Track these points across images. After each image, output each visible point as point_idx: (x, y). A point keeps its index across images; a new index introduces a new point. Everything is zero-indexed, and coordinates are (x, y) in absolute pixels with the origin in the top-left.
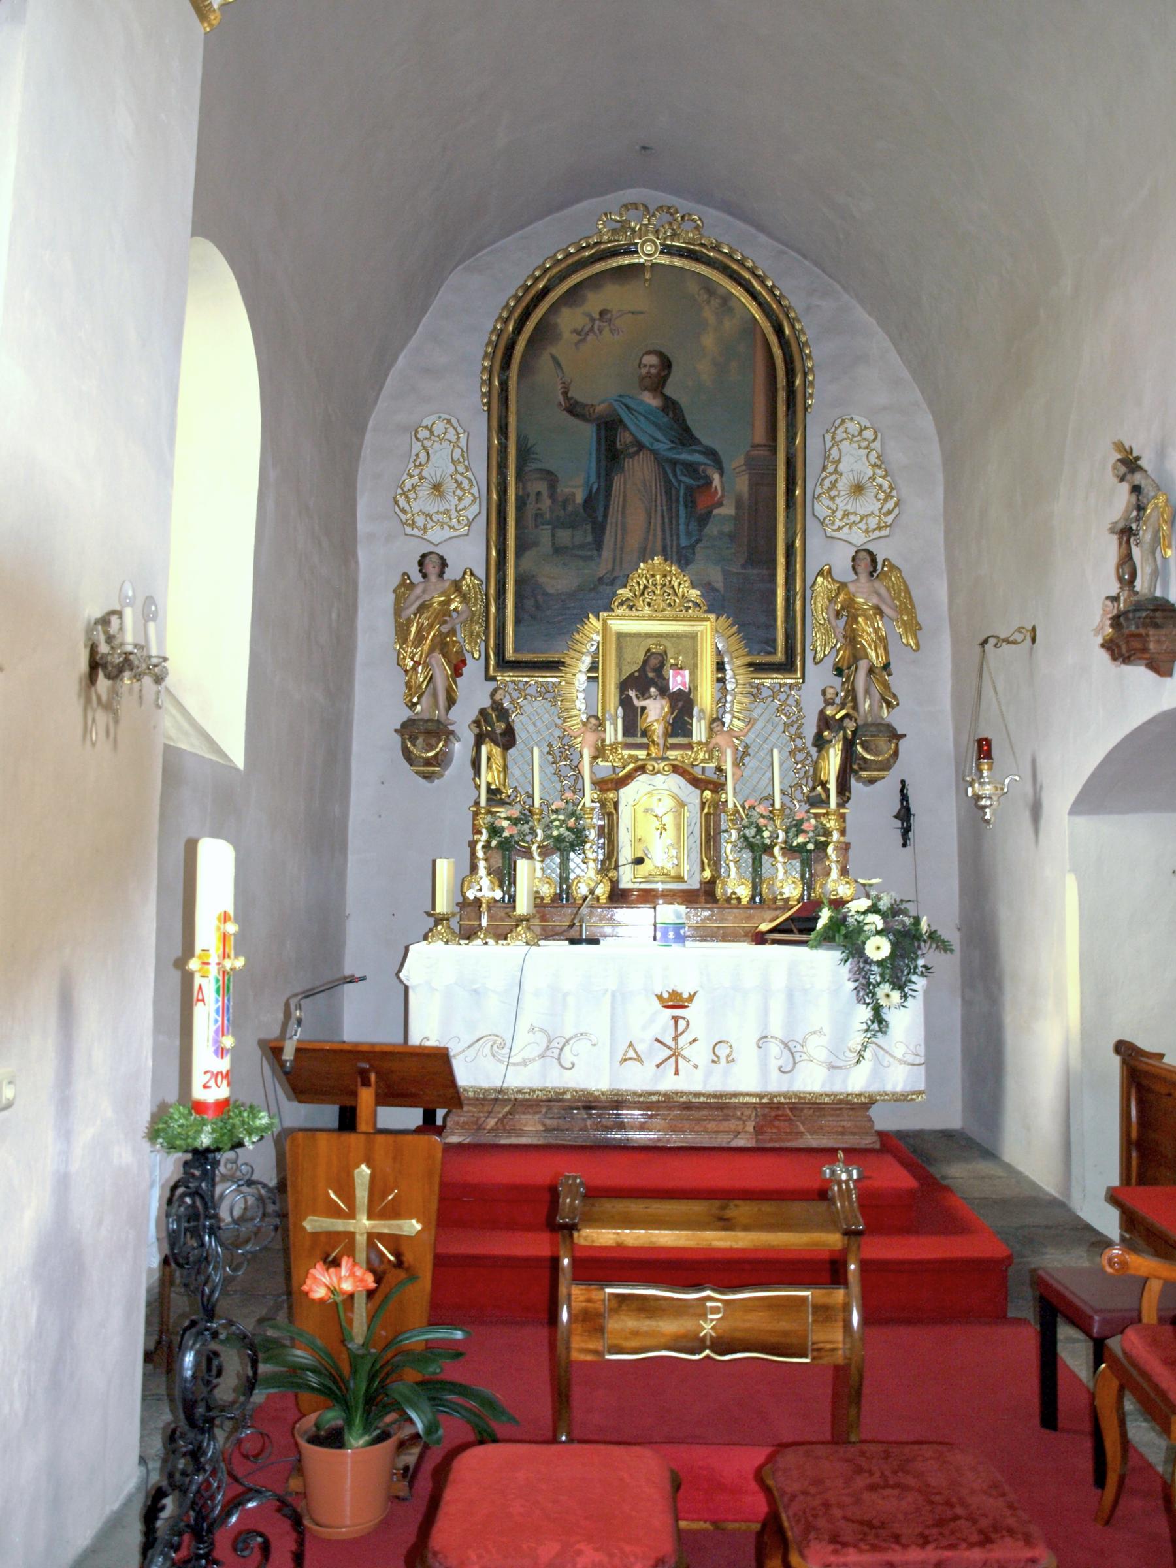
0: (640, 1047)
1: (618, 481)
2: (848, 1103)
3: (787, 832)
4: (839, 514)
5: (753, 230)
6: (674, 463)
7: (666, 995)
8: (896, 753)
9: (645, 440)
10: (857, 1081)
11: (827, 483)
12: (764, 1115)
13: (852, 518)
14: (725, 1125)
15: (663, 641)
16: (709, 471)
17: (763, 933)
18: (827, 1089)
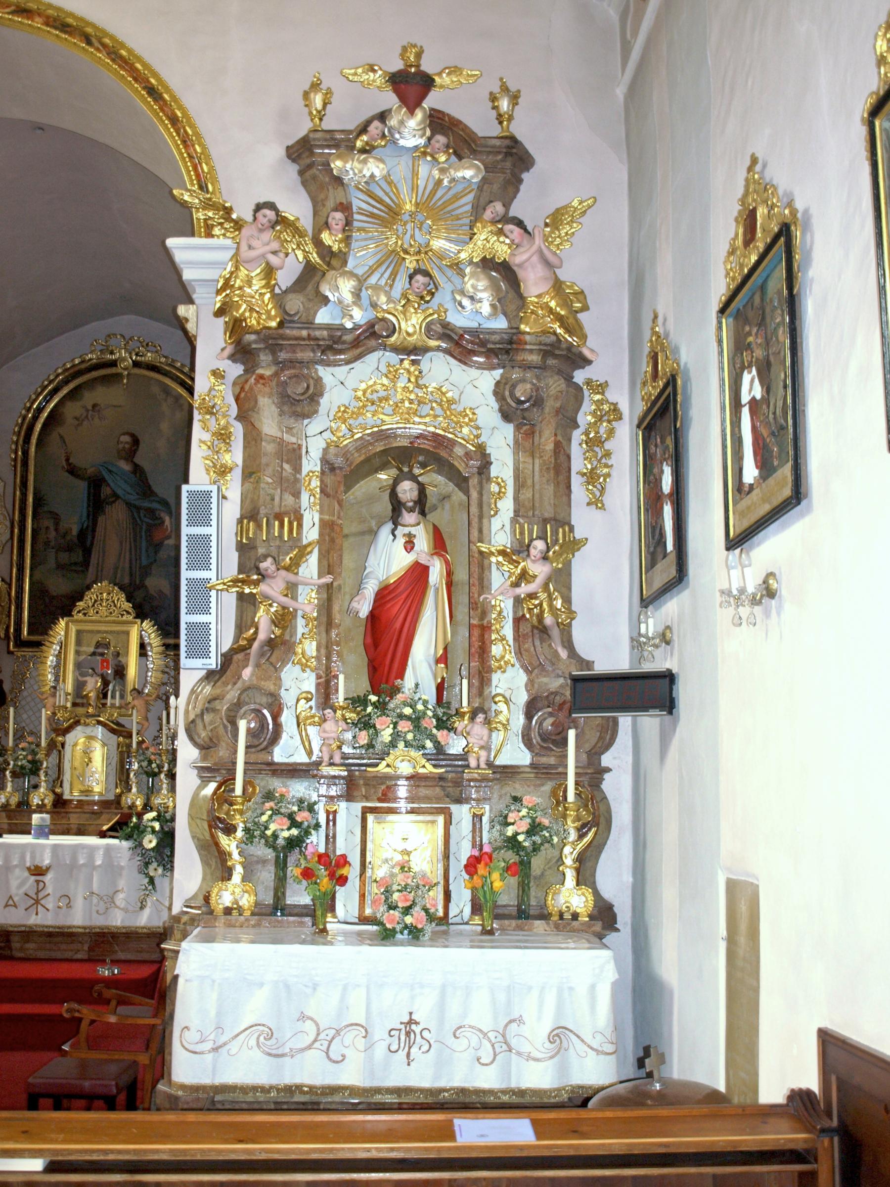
0: (16, 899)
1: (101, 520)
2: (137, 933)
6: (138, 509)
7: (33, 868)
9: (119, 492)
12: (96, 940)
14: (71, 946)
16: (162, 515)
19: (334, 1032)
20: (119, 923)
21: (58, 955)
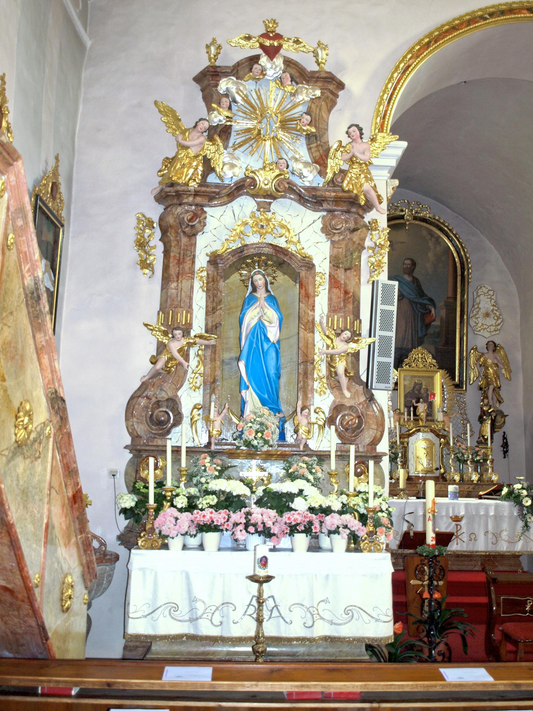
3: (472, 455)
4: (480, 325)
5: (445, 208)
8: (504, 422)
10: (519, 547)
11: (475, 312)
13: (485, 326)
15: (421, 379)
16: (430, 307)
17: (481, 495)
18: (508, 550)
19: (215, 608)
20: (505, 549)
21: (464, 568)
